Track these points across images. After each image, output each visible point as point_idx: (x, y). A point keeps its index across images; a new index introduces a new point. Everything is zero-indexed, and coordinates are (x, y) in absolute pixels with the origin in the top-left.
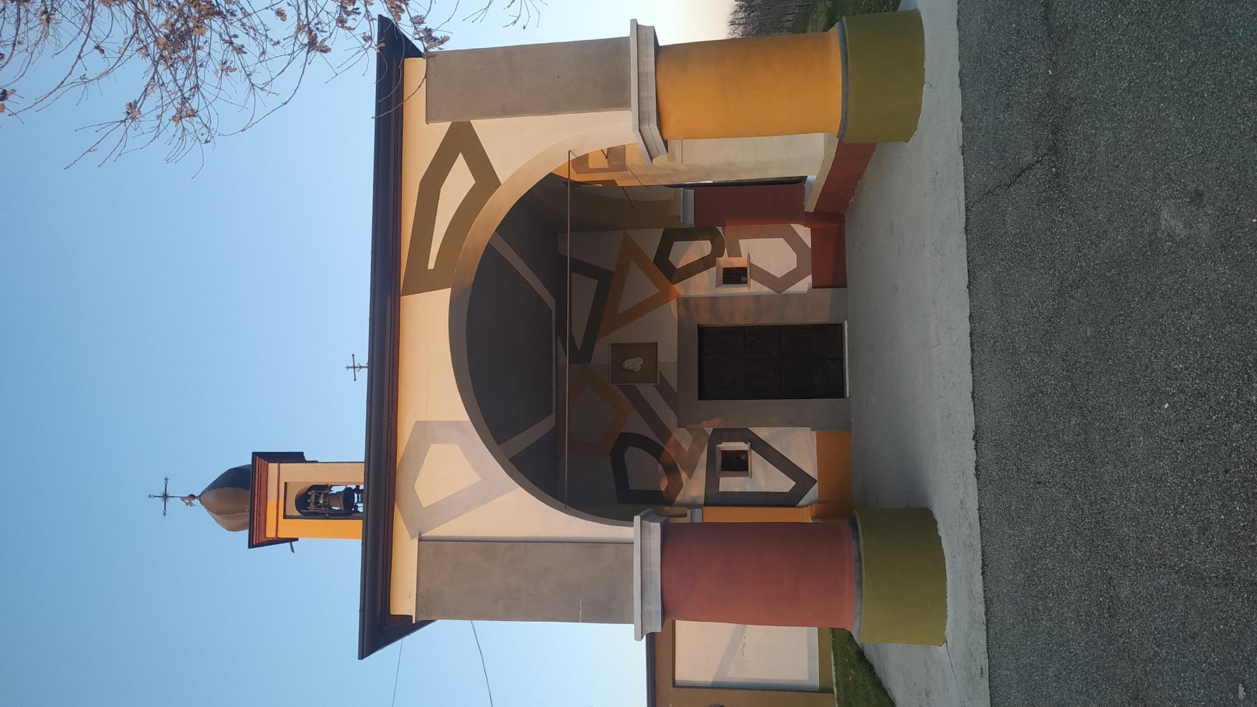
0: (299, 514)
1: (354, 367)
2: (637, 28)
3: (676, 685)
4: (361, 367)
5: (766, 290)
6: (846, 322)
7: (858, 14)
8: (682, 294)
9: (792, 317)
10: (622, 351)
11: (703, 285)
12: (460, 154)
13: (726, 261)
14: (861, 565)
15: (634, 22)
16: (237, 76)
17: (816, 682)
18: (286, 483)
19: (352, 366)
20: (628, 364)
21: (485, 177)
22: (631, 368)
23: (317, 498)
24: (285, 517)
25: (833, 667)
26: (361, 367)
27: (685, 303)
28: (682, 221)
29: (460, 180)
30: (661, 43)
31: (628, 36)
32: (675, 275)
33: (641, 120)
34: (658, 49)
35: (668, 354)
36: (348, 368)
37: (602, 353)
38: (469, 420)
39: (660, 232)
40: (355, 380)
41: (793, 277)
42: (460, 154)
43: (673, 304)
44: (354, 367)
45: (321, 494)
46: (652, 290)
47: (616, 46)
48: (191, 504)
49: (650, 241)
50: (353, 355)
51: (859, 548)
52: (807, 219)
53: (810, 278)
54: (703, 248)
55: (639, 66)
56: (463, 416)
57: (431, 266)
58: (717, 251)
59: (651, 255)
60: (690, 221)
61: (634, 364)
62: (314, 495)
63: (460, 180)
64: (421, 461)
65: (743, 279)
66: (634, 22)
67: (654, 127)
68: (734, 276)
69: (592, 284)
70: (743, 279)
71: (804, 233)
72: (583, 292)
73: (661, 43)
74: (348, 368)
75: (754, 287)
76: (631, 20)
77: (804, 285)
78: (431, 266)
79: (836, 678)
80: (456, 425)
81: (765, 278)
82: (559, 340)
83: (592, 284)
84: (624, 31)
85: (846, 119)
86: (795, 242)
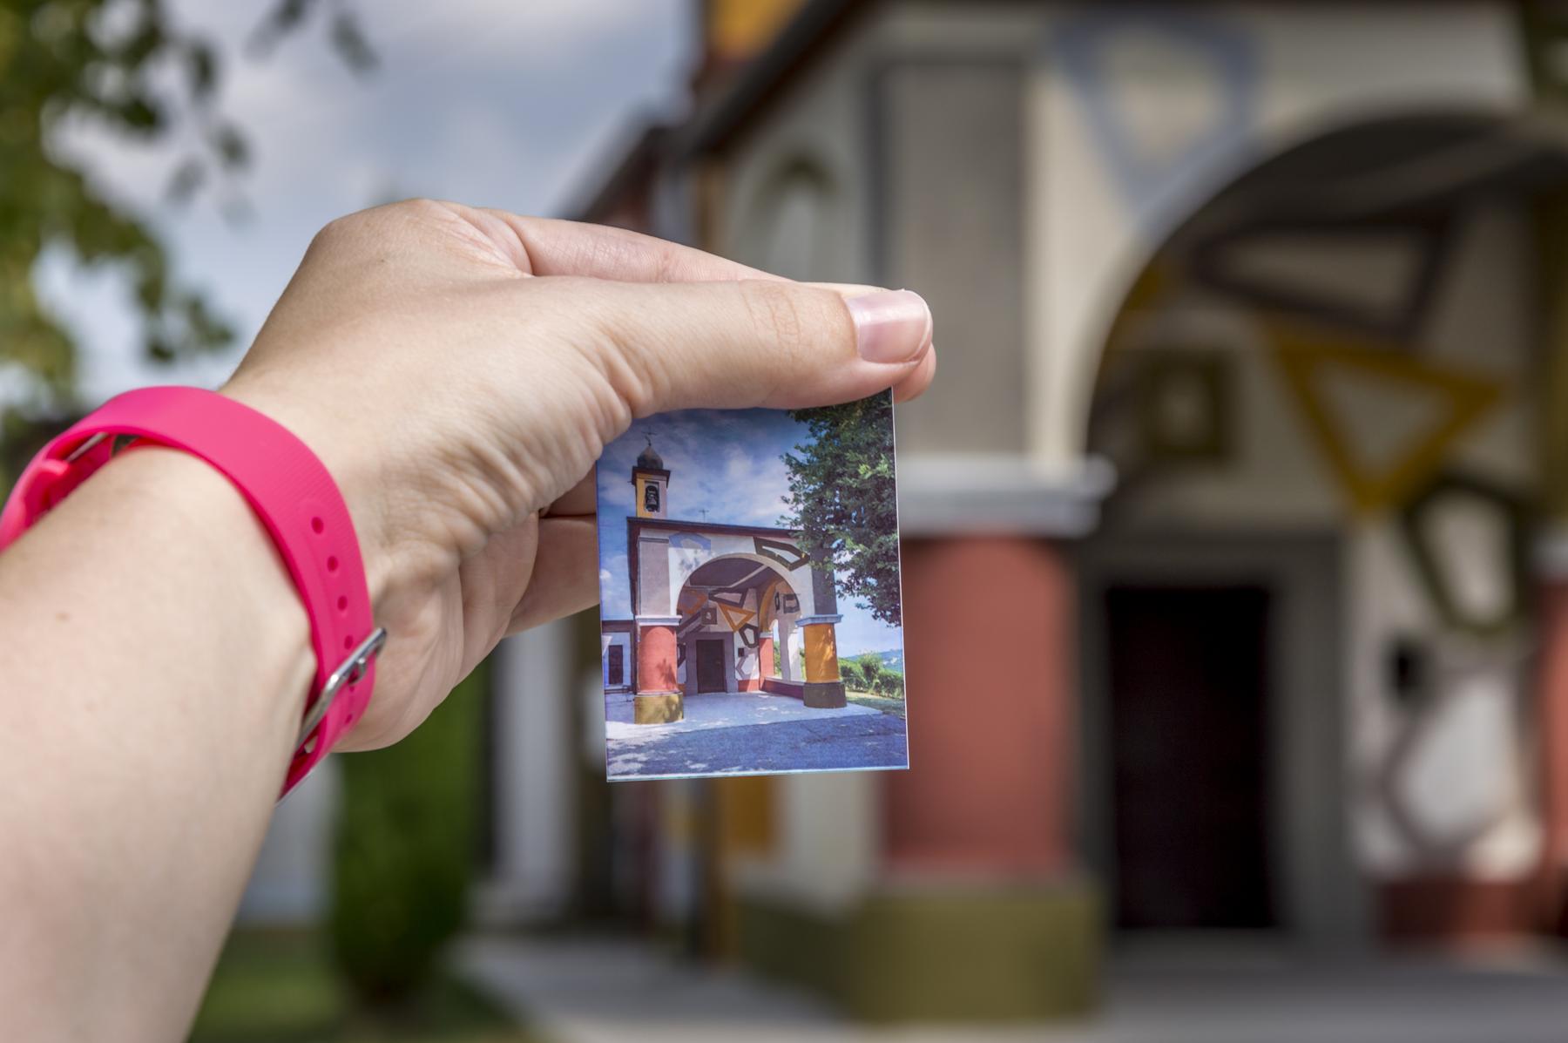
2: (841, 617)
5: (736, 664)
7: (792, 493)
10: (714, 611)
11: (739, 643)
13: (1449, 652)
20: (709, 614)
21: (793, 567)
33: (813, 619)
34: (833, 624)
35: (714, 628)
37: (712, 604)
46: (736, 623)
47: (835, 611)
49: (753, 622)
54: (751, 640)
55: (829, 618)
57: (764, 547)
61: (709, 616)
63: (791, 558)
68: (741, 652)
69: (738, 601)
72: (735, 597)
75: (737, 660)
77: (738, 677)
78: (764, 547)
81: (1402, 749)
83: (738, 601)
84: (839, 613)
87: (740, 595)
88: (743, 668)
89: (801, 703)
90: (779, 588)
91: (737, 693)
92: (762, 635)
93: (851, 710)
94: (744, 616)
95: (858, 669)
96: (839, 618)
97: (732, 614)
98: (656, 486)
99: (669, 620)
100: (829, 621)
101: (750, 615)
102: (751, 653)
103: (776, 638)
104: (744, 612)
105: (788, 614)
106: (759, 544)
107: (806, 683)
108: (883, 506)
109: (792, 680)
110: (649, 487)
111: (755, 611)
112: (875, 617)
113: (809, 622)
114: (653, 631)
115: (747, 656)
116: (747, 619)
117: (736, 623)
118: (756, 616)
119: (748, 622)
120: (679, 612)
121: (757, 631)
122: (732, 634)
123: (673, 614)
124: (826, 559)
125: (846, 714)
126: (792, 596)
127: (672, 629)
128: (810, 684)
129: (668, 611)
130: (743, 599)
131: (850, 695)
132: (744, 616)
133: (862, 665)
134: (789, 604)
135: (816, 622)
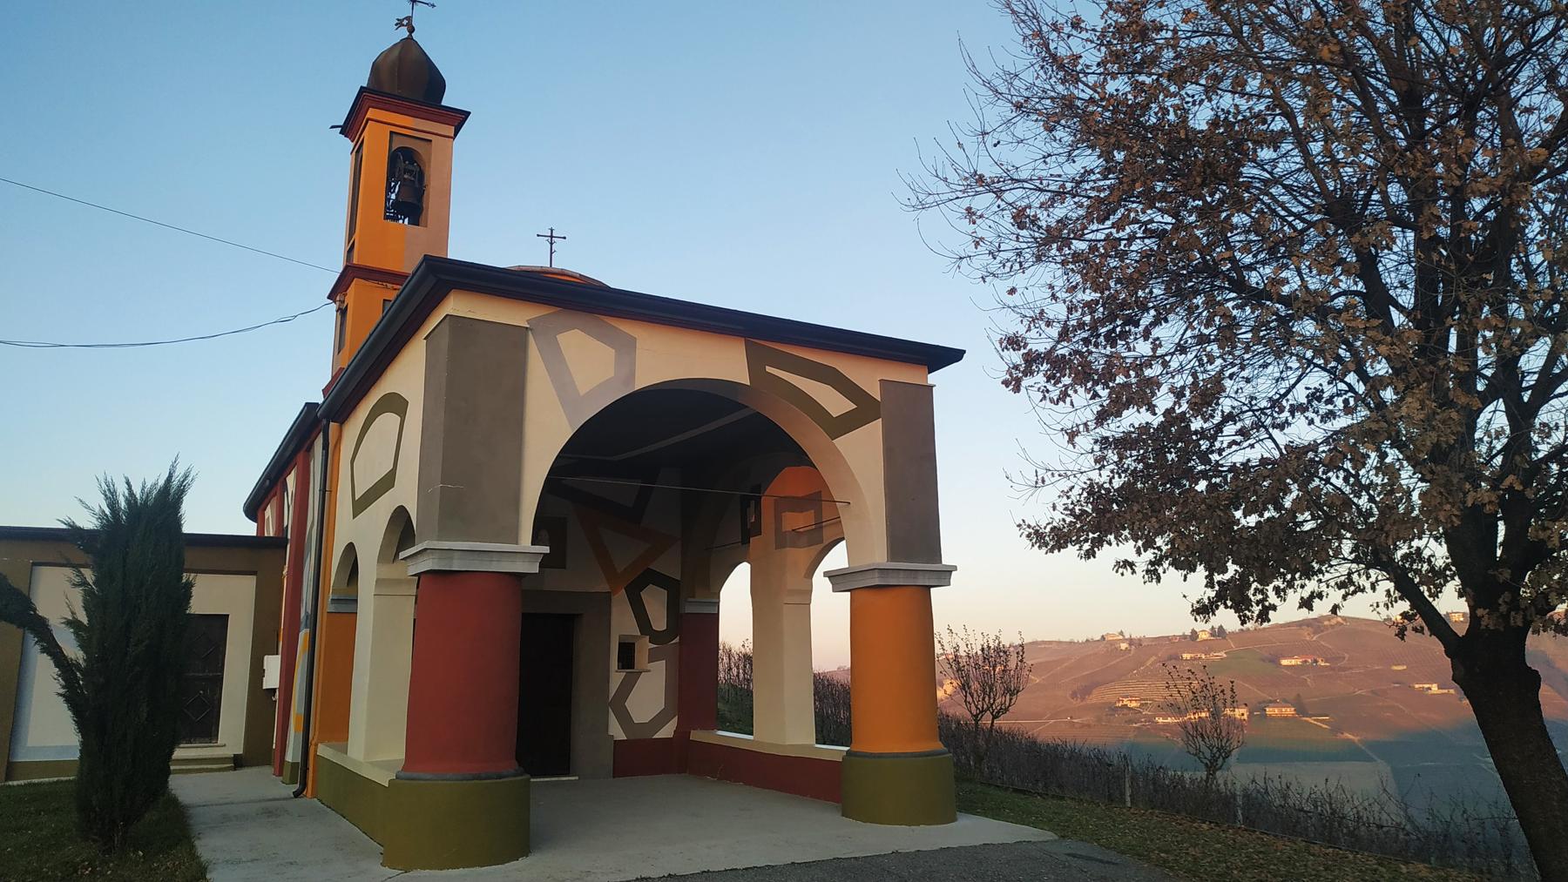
0: (393, 149)
1: (552, 237)
3: (34, 567)
4: (551, 244)
6: (577, 778)
8: (615, 598)
11: (623, 623)
12: (855, 407)
13: (644, 646)
14: (493, 778)
15: (955, 568)
16: (971, 249)
17: (22, 756)
18: (431, 141)
23: (410, 172)
24: (391, 133)
25: (55, 779)
26: (551, 244)
27: (606, 599)
28: (690, 600)
29: (836, 404)
30: (932, 589)
31: (944, 563)
33: (883, 571)
34: (929, 587)
36: (552, 230)
40: (538, 235)
41: (625, 718)
42: (855, 407)
43: (604, 587)
44: (552, 237)
47: (934, 552)
48: (400, 24)
49: (669, 565)
52: (681, 733)
54: (659, 623)
56: (641, 383)
57: (768, 369)
58: (656, 637)
59: (657, 566)
60: (689, 609)
62: (413, 168)
63: (836, 404)
66: (955, 568)
67: (877, 582)
71: (667, 731)
73: (932, 589)
74: (552, 230)
75: (617, 678)
76: (956, 567)
77: (617, 732)
79: (38, 784)
80: (631, 376)
81: (627, 688)
84: (947, 559)
85: (874, 757)
86: (660, 720)
88: (629, 704)
96: (944, 576)
113: (876, 580)
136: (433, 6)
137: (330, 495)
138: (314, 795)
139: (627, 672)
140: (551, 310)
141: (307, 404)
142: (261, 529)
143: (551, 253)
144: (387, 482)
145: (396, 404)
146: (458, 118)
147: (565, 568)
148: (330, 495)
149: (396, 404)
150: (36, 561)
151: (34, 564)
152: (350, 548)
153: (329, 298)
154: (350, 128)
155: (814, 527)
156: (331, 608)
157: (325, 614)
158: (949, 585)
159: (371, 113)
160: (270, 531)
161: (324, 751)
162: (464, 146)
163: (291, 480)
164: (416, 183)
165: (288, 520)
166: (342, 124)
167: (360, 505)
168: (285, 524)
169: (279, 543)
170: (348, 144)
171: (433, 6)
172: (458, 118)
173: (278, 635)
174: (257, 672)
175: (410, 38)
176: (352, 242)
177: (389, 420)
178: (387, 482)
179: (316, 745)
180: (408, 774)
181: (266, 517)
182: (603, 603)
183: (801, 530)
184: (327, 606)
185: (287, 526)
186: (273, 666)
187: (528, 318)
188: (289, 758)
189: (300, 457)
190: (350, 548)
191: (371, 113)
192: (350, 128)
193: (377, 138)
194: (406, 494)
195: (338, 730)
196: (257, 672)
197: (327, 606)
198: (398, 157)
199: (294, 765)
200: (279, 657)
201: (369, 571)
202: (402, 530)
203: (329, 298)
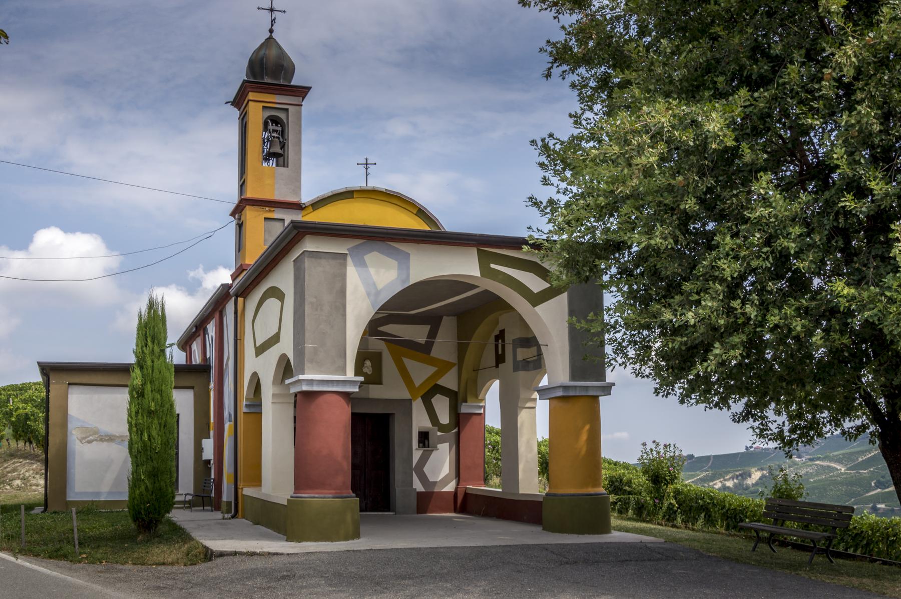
1: (367, 164)
4: (367, 169)
9: (398, 476)
11: (420, 420)
19: (365, 163)
22: (365, 365)
26: (367, 169)
32: (427, 400)
33: (565, 388)
34: (596, 398)
36: (367, 159)
38: (410, 284)
39: (455, 388)
40: (358, 164)
41: (423, 478)
43: (406, 395)
44: (367, 164)
45: (279, 134)
46: (418, 383)
47: (602, 376)
49: (449, 381)
50: (375, 164)
51: (329, 498)
53: (423, 490)
54: (444, 418)
56: (413, 280)
57: (492, 266)
58: (442, 428)
63: (536, 284)
64: (388, 255)
65: (421, 445)
66: (614, 384)
69: (422, 339)
70: (421, 445)
74: (367, 159)
75: (417, 455)
77: (418, 486)
78: (492, 266)
81: (424, 460)
82: (385, 315)
86: (445, 481)
87: (426, 329)
88: (427, 469)
89: (540, 529)
90: (504, 321)
91: (416, 515)
92: (464, 409)
93: (615, 536)
94: (432, 370)
95: (641, 480)
96: (607, 389)
97: (409, 363)
98: (282, 115)
99: (344, 382)
100: (591, 393)
101: (443, 367)
102: (442, 441)
103: (493, 419)
104: (433, 362)
105: (521, 374)
106: (485, 259)
107: (547, 495)
108: (709, 77)
109: (521, 492)
110: (270, 117)
111: (453, 359)
112: (657, 392)
113: (560, 393)
114: (321, 399)
115: (436, 448)
116: (439, 374)
117: (418, 383)
118: (454, 370)
119: (440, 382)
120: (357, 373)
121: (456, 399)
122: (409, 402)
123: (350, 374)
124: (591, 316)
125: (608, 540)
126: (530, 341)
127: (346, 395)
128: (555, 495)
129: (344, 371)
130: (432, 334)
131: (614, 521)
132: (432, 370)
133: (645, 472)
134: (523, 354)
135: (571, 393)
136: (284, 12)
137: (240, 342)
138: (243, 517)
139: (424, 450)
140: (358, 242)
141: (222, 285)
142: (189, 357)
143: (367, 175)
144: (275, 339)
145: (276, 293)
146: (302, 92)
147: (380, 383)
148: (240, 342)
149: (276, 293)
150: (71, 382)
151: (69, 384)
152: (255, 375)
153: (231, 215)
154: (239, 101)
155: (536, 358)
156: (245, 410)
157: (242, 413)
158: (610, 394)
159: (251, 96)
160: (197, 359)
161: (248, 491)
162: (309, 105)
163: (211, 328)
164: (280, 137)
165: (211, 353)
166: (232, 100)
167: (260, 350)
168: (208, 356)
169: (204, 369)
170: (236, 113)
171: (284, 12)
172: (302, 92)
173: (209, 426)
174: (198, 449)
175: (270, 38)
176: (243, 180)
177: (272, 304)
178: (275, 339)
179: (242, 489)
180: (295, 495)
181: (193, 350)
182: (406, 405)
183: (529, 360)
184: (243, 409)
185: (210, 358)
186: (208, 445)
187: (349, 247)
188: (224, 498)
189: (217, 315)
190: (255, 375)
191: (251, 96)
192: (239, 101)
193: (256, 114)
194: (286, 346)
195: (256, 480)
196: (198, 449)
197: (243, 409)
198: (268, 122)
199: (229, 503)
200: (568, 382)
201: (268, 391)
202: (286, 369)
203: (231, 215)
